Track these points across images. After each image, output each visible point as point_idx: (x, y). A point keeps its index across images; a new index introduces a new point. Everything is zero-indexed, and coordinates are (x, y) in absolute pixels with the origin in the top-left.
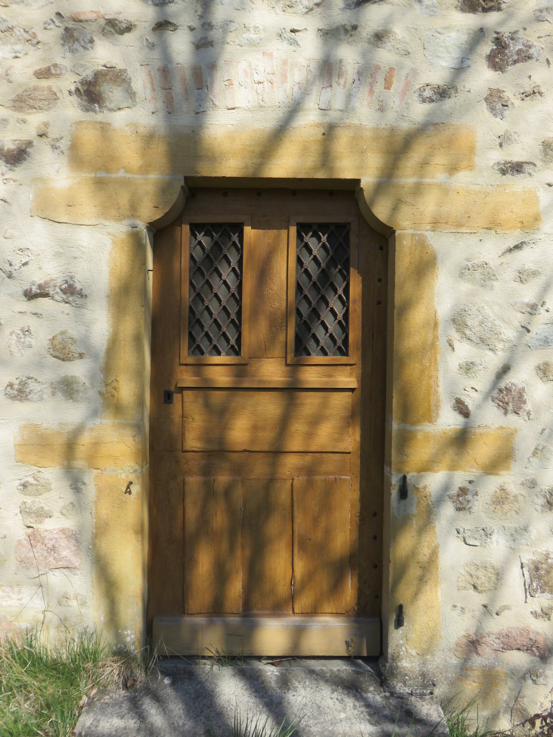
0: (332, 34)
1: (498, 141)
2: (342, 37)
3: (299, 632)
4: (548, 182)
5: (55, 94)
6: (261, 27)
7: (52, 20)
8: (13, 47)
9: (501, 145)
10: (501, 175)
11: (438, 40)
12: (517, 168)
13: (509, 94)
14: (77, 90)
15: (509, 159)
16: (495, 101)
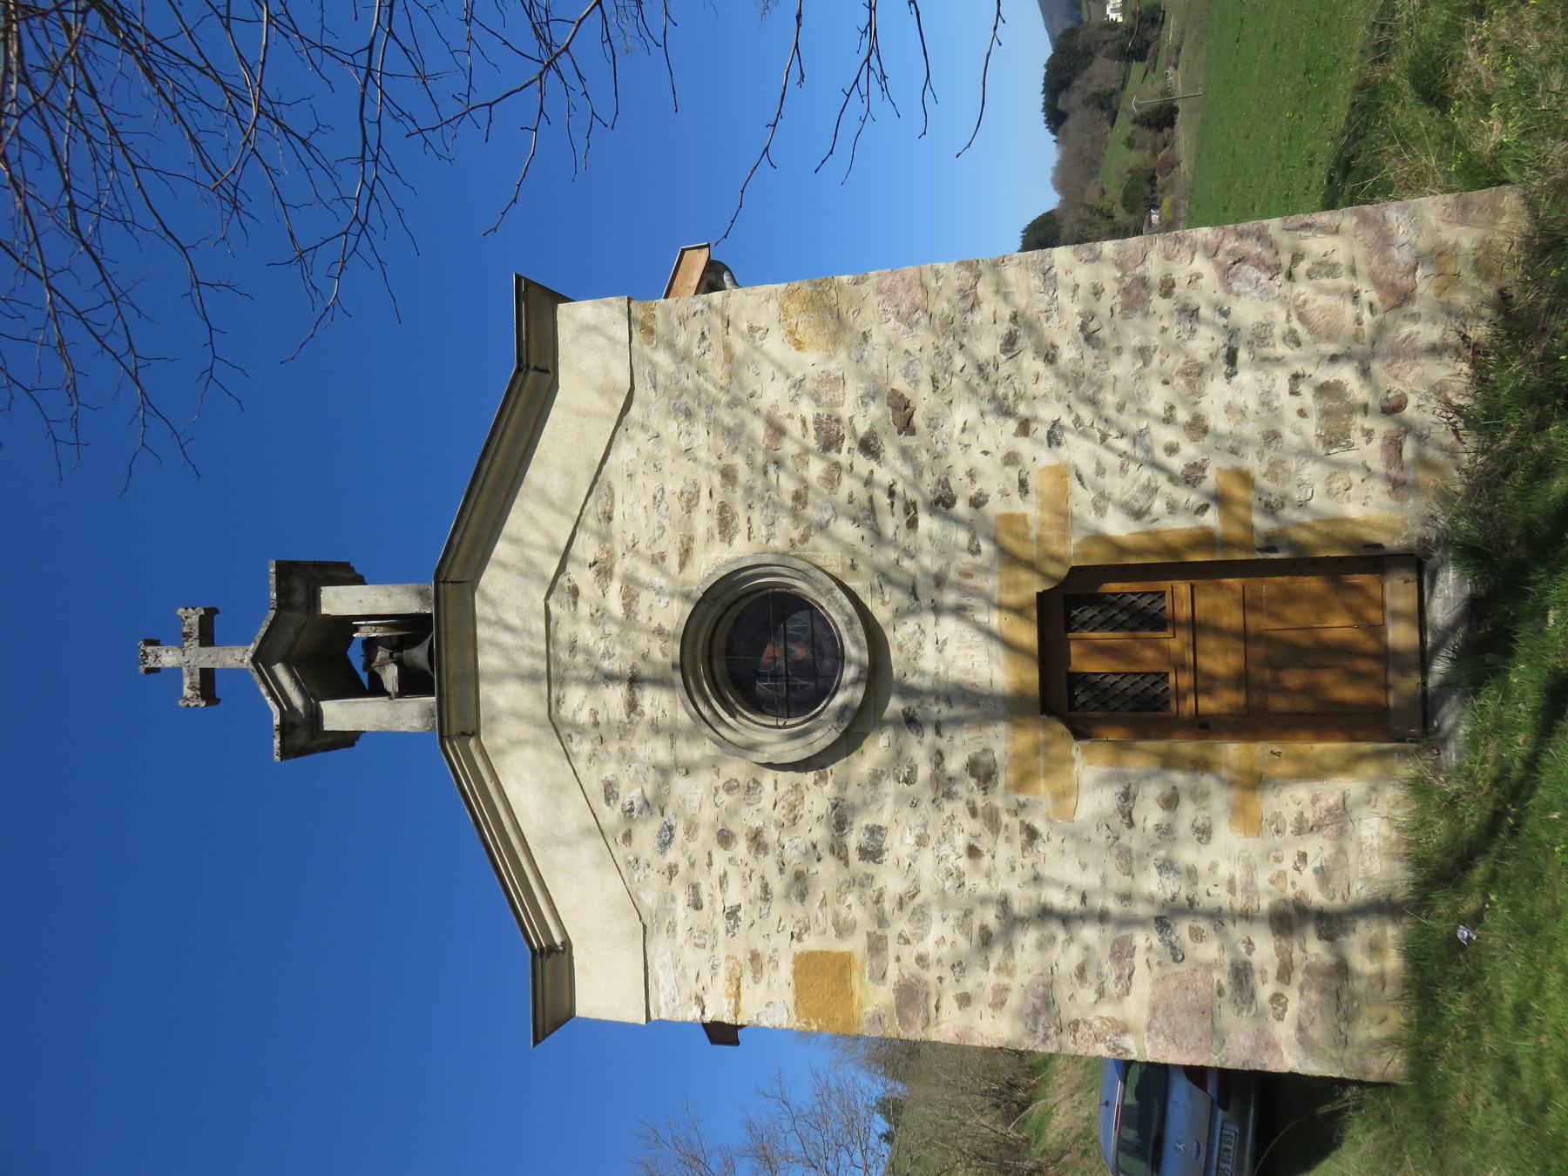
0: (937, 610)
3: (1397, 615)
12: (1023, 485)
16: (977, 502)
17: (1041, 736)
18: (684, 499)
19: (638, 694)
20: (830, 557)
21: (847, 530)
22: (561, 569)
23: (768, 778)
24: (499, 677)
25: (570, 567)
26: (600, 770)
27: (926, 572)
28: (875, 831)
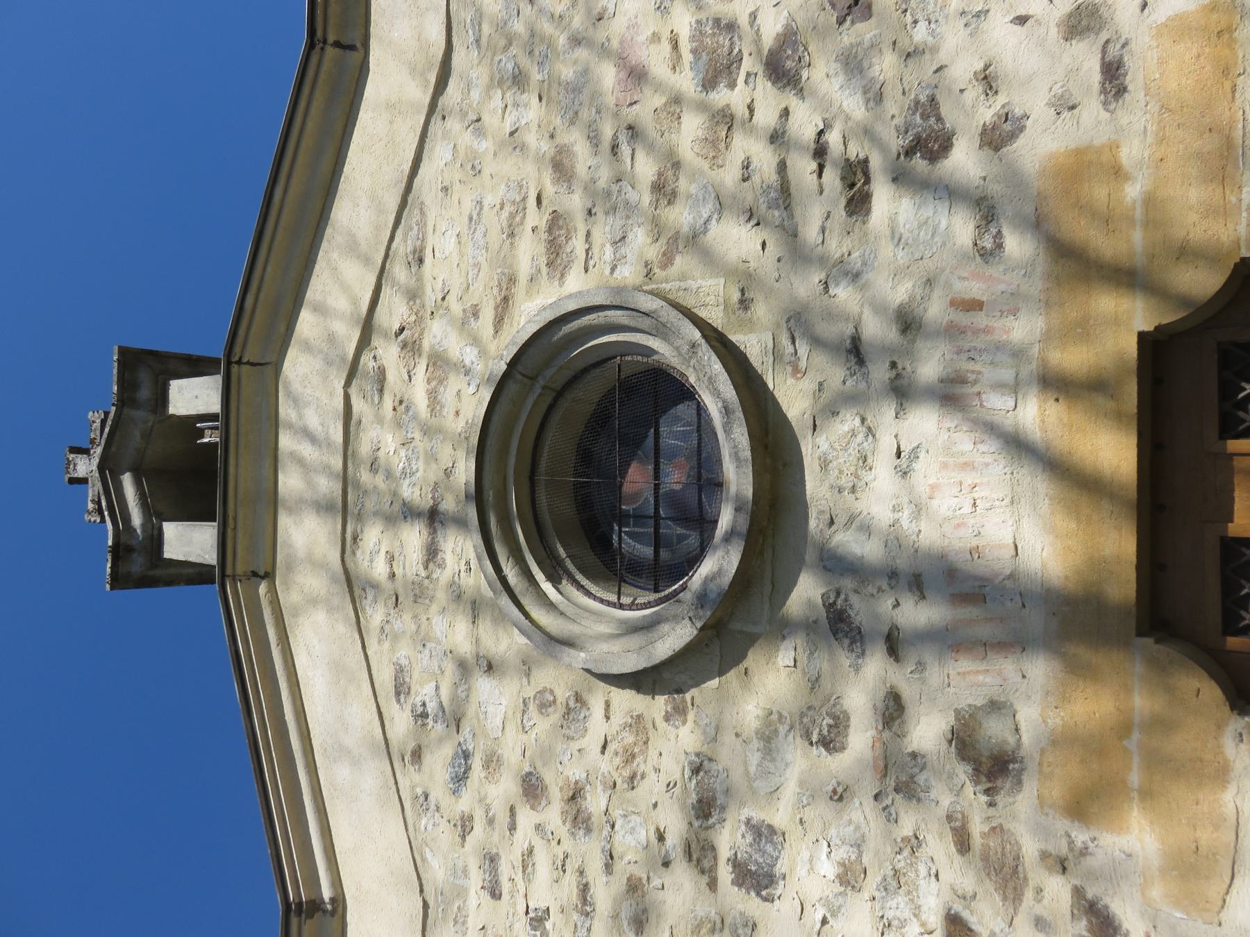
0: (902, 392)
1: (1066, 114)
2: (905, 382)
4: (1138, 10)
5: (993, 829)
6: (894, 502)
7: (884, 809)
8: (922, 876)
9: (1073, 108)
10: (1126, 95)
11: (910, 241)
13: (987, 114)
14: (987, 792)
15: (1096, 87)
16: (996, 138)
17: (1141, 702)
18: (505, 214)
19: (440, 538)
20: (710, 295)
21: (738, 240)
22: (365, 341)
23: (599, 695)
24: (298, 506)
25: (376, 341)
26: (393, 649)
27: (879, 308)
28: (762, 833)
